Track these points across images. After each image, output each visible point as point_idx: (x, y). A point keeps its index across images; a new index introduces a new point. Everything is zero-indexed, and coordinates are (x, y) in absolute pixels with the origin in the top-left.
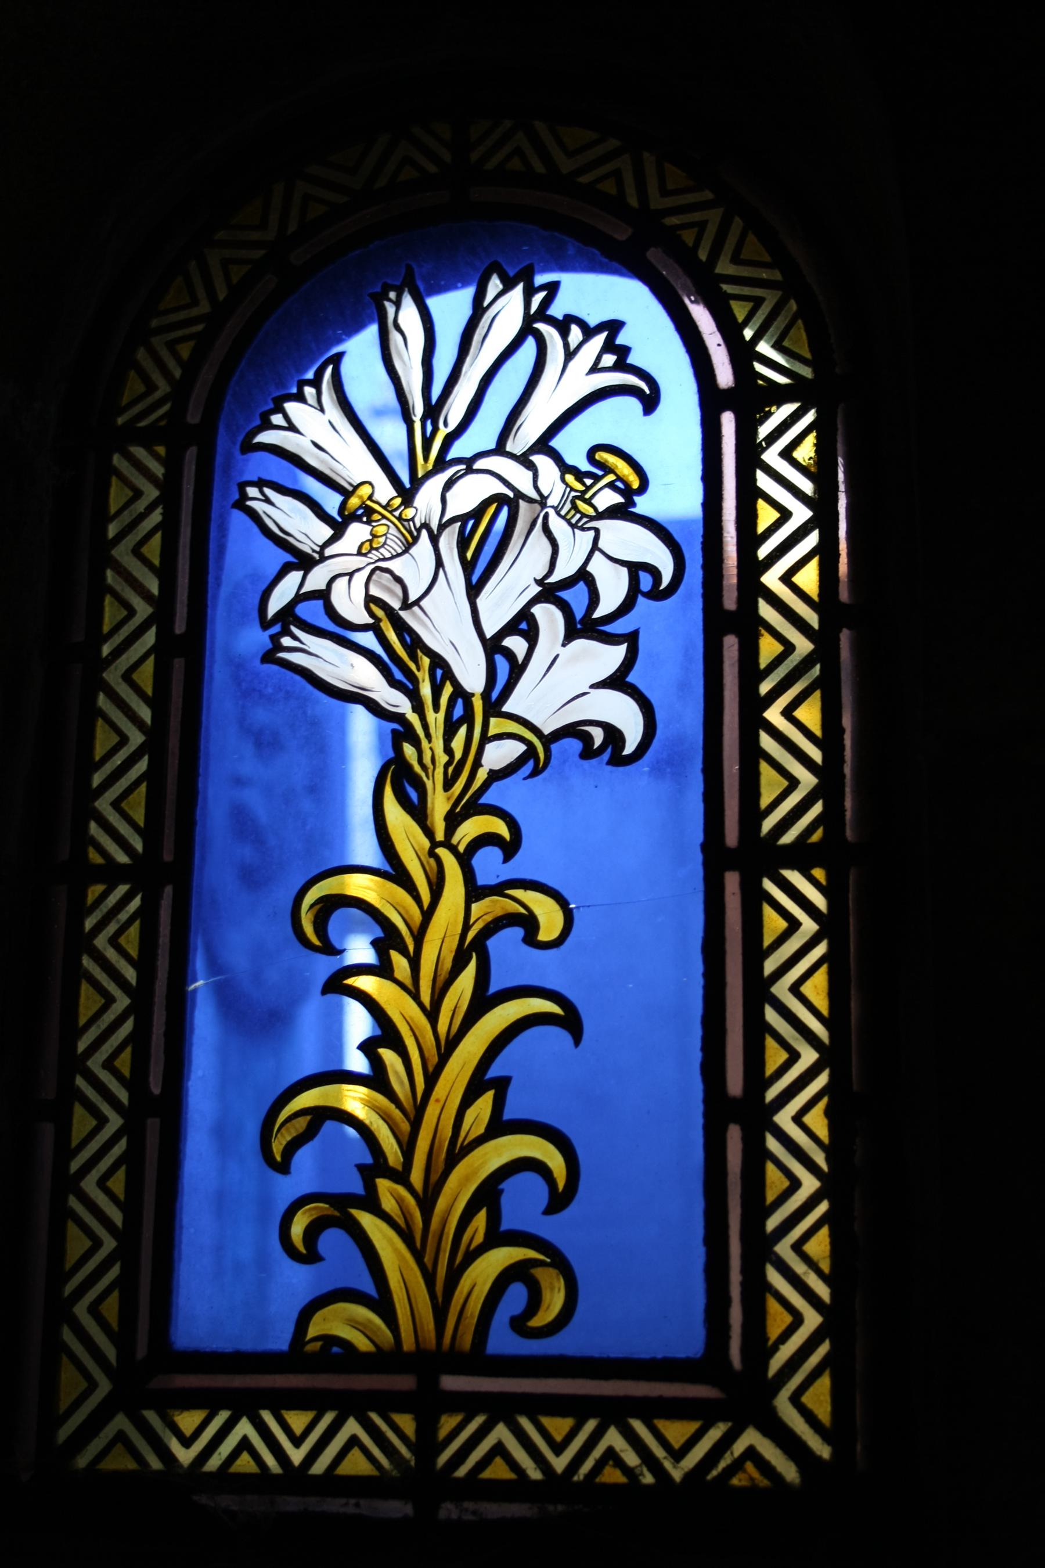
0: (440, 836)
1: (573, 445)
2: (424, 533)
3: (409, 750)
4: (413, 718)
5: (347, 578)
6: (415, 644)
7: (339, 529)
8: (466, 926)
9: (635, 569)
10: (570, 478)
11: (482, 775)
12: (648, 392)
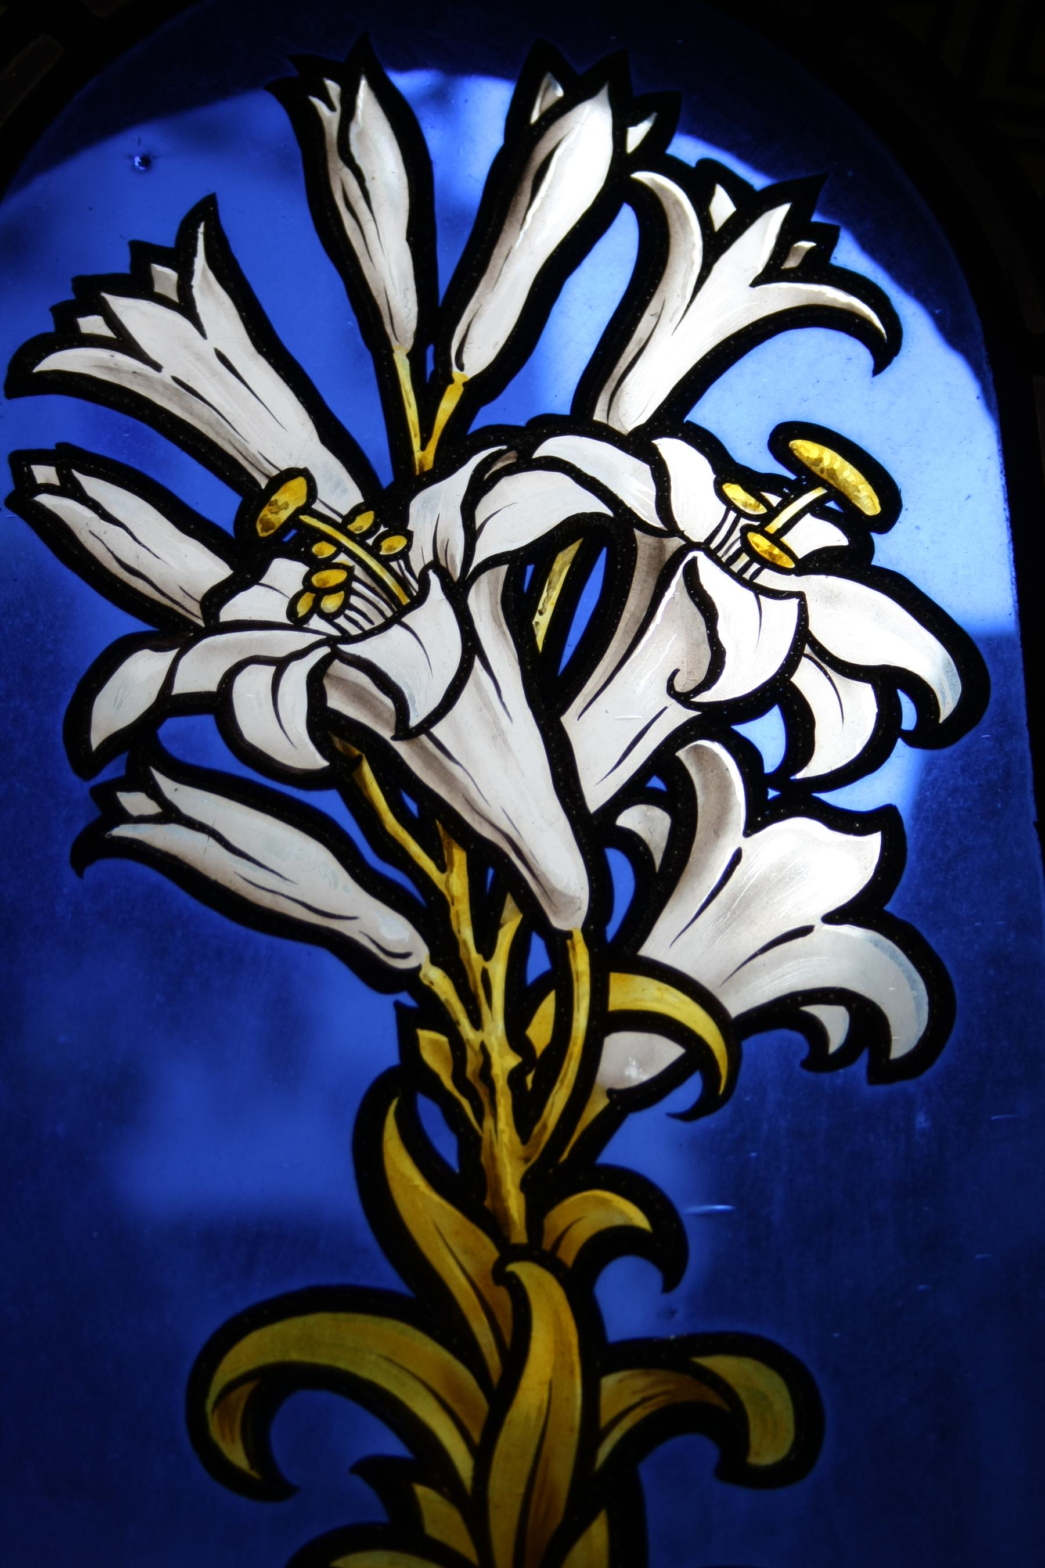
0: (519, 1235)
1: (741, 413)
2: (434, 580)
3: (431, 1044)
4: (437, 979)
5: (272, 669)
6: (439, 821)
7: (247, 571)
8: (591, 1430)
9: (889, 682)
10: (735, 492)
11: (597, 1104)
12: (610, 513)
